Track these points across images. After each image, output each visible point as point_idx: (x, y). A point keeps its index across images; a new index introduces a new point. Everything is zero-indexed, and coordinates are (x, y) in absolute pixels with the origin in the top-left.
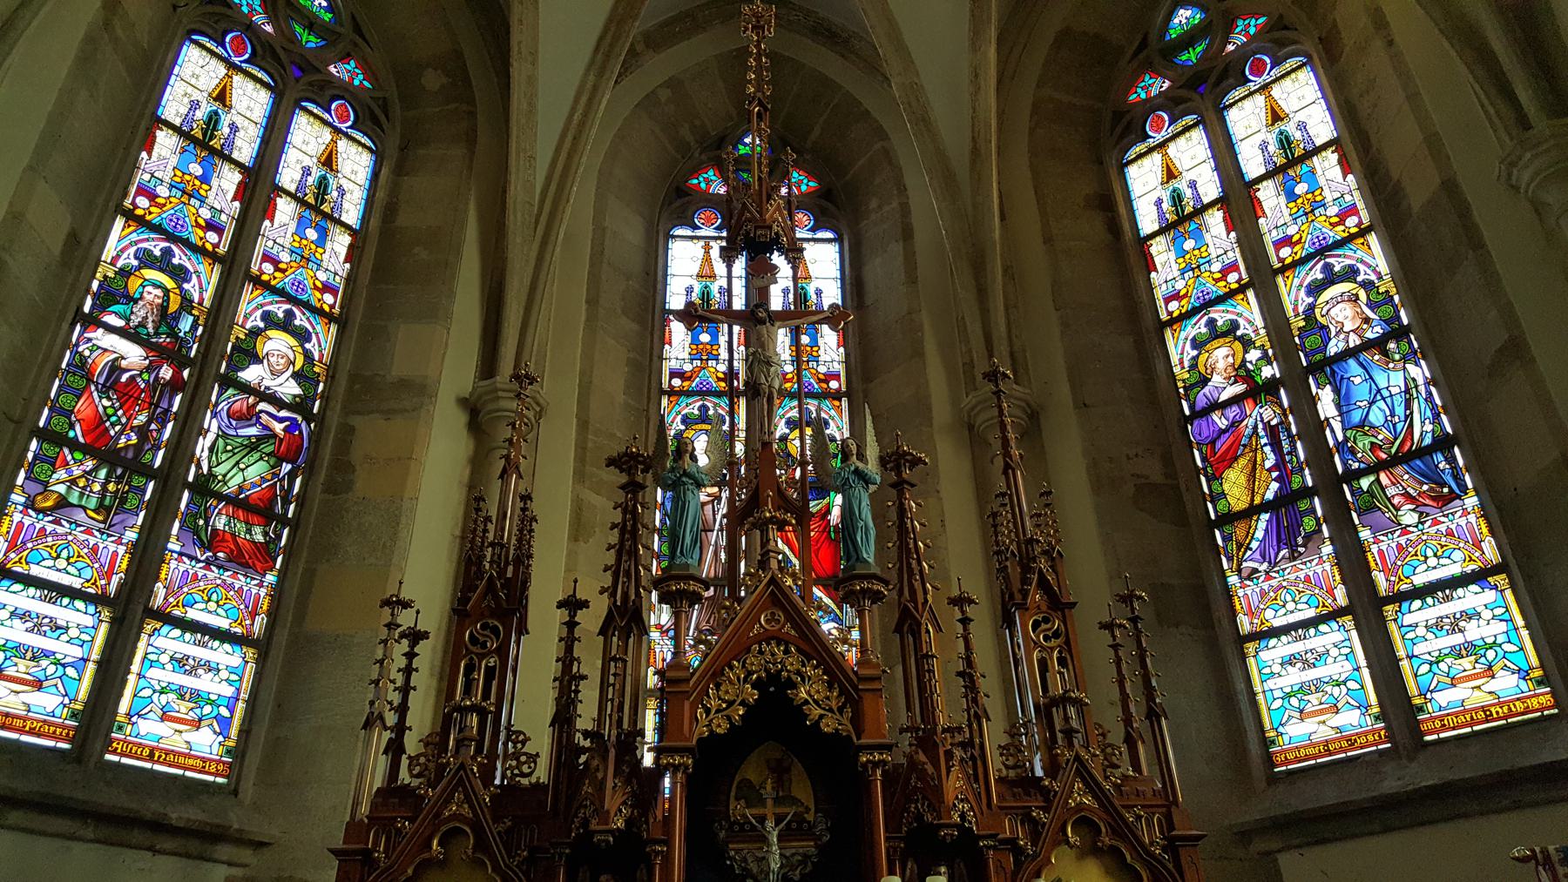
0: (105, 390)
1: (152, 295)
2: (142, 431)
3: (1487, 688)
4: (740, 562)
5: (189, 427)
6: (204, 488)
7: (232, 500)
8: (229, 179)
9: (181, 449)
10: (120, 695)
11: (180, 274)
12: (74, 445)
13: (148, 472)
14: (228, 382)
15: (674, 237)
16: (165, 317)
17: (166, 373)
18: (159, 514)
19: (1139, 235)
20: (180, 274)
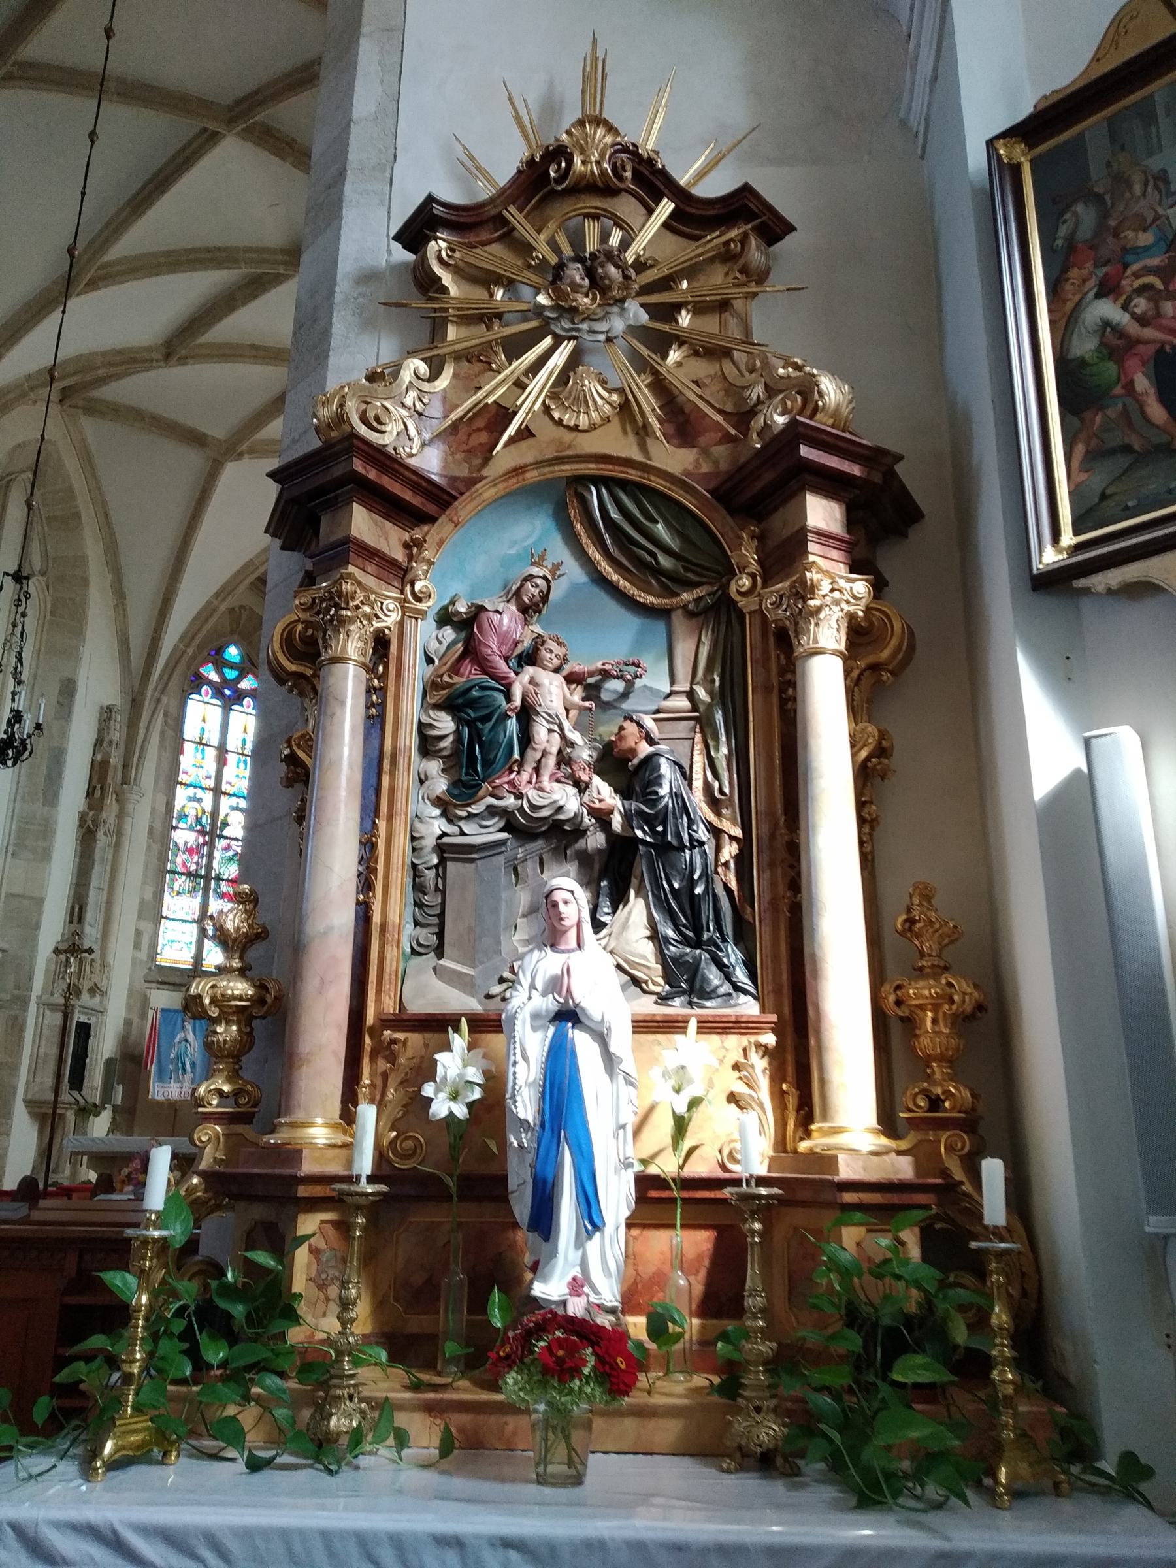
0: (184, 852)
1: (193, 812)
2: (197, 863)
3: (456, 830)
4: (872, 1528)
5: (210, 857)
6: (218, 878)
7: (227, 880)
8: (211, 753)
9: (209, 867)
10: (1132, 92)
11: (199, 801)
12: (179, 873)
13: (201, 877)
14: (221, 836)
15: (281, 1124)
16: (198, 820)
17: (201, 840)
18: (206, 890)
19: (153, 951)
20: (199, 801)
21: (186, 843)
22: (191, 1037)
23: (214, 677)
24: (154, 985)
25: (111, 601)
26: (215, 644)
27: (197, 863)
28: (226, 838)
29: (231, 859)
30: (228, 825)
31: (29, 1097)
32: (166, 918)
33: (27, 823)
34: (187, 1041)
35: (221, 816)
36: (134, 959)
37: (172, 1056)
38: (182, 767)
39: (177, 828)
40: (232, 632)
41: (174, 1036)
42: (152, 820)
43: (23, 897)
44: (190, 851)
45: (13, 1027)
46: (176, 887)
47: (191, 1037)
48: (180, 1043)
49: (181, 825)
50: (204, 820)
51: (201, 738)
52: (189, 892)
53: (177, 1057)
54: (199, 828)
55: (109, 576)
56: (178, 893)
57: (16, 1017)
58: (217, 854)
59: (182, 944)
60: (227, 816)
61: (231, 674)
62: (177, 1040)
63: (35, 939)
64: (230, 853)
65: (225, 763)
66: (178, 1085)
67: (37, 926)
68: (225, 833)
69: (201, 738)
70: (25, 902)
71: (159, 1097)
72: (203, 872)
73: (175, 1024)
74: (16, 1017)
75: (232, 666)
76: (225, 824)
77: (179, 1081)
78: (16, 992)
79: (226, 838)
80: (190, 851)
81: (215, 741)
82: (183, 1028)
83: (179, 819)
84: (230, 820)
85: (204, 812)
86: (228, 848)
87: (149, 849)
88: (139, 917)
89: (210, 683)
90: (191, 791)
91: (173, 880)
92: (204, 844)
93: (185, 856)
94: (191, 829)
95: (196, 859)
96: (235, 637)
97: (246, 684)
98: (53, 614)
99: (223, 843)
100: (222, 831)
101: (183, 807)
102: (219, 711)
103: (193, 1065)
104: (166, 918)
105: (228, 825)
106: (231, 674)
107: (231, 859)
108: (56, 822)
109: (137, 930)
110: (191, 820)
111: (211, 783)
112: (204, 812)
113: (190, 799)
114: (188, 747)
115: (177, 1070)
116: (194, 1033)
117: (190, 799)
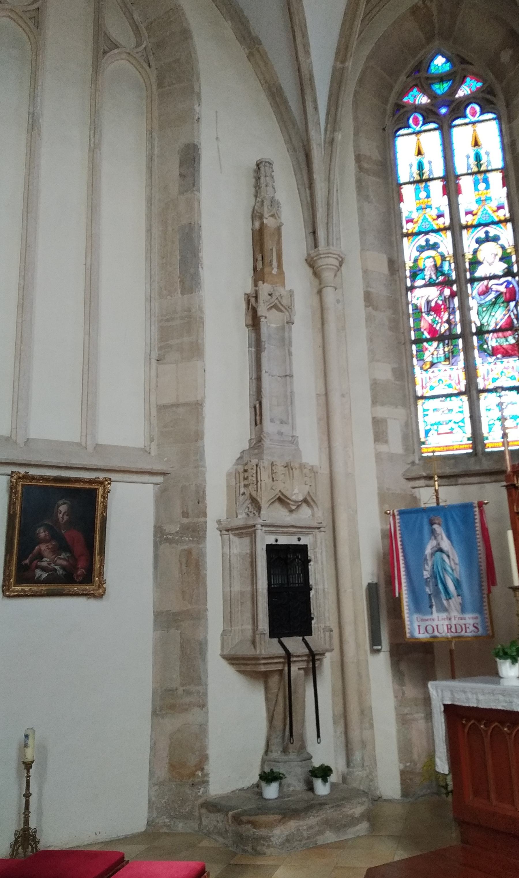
0: (428, 313)
1: (429, 263)
2: (448, 322)
5: (464, 309)
7: (494, 331)
8: (437, 187)
9: (465, 321)
12: (427, 340)
14: (473, 280)
17: (447, 292)
18: (468, 349)
20: (435, 247)
21: (428, 302)
22: (445, 544)
23: (424, 100)
24: (422, 482)
25: (241, 52)
26: (412, 64)
27: (448, 322)
28: (481, 279)
29: (494, 304)
30: (479, 263)
31: (226, 652)
32: (423, 397)
33: (168, 320)
34: (441, 550)
35: (469, 255)
36: (378, 457)
37: (426, 574)
38: (405, 215)
39: (412, 288)
40: (430, 39)
41: (421, 547)
42: (367, 284)
43: (177, 405)
44: (436, 310)
45: (187, 565)
46: (427, 357)
47: (445, 544)
48: (433, 554)
49: (419, 282)
50: (446, 267)
51: (421, 174)
52: (447, 359)
53: (434, 575)
54: (441, 278)
55: (228, 25)
56: (432, 364)
57: (189, 552)
58: (473, 303)
59: (451, 425)
60: (475, 252)
61: (440, 88)
62: (428, 551)
63: (200, 453)
64: (492, 296)
65: (458, 191)
66: (444, 615)
67: (198, 436)
68: (478, 274)
69: (421, 174)
70: (181, 410)
71: (421, 635)
72: (458, 330)
73: (421, 530)
74: (189, 552)
75: (441, 78)
76: (475, 263)
77: (445, 610)
78: (185, 521)
79: (481, 279)
80: (436, 310)
81: (439, 170)
82: (433, 532)
83: (414, 276)
84: (480, 256)
85: (443, 258)
86: (486, 291)
87: (369, 319)
88: (374, 402)
89: (417, 108)
90: (421, 240)
91: (421, 351)
92: (453, 295)
93: (429, 319)
94: (430, 284)
95: (445, 316)
96: (437, 43)
97: (463, 91)
98: (160, 85)
99: (479, 286)
100: (472, 273)
101: (416, 261)
102: (437, 134)
103: (458, 584)
104: (423, 397)
105: (479, 263)
106: (440, 88)
107: (494, 304)
108: (201, 309)
109: (374, 418)
110: (429, 273)
111: (446, 221)
112: (443, 258)
113: (421, 249)
114: (408, 191)
115: (437, 593)
116: (449, 537)
117: (421, 249)
